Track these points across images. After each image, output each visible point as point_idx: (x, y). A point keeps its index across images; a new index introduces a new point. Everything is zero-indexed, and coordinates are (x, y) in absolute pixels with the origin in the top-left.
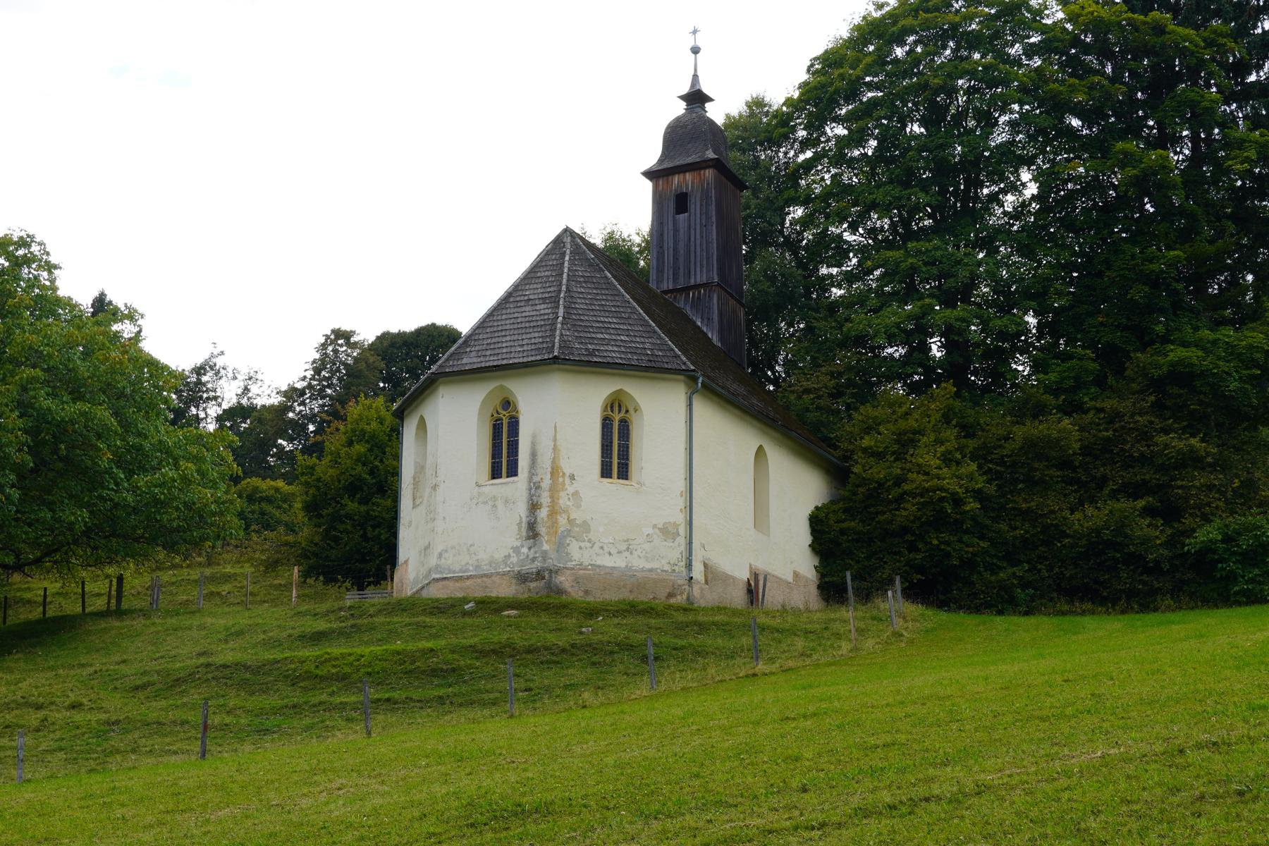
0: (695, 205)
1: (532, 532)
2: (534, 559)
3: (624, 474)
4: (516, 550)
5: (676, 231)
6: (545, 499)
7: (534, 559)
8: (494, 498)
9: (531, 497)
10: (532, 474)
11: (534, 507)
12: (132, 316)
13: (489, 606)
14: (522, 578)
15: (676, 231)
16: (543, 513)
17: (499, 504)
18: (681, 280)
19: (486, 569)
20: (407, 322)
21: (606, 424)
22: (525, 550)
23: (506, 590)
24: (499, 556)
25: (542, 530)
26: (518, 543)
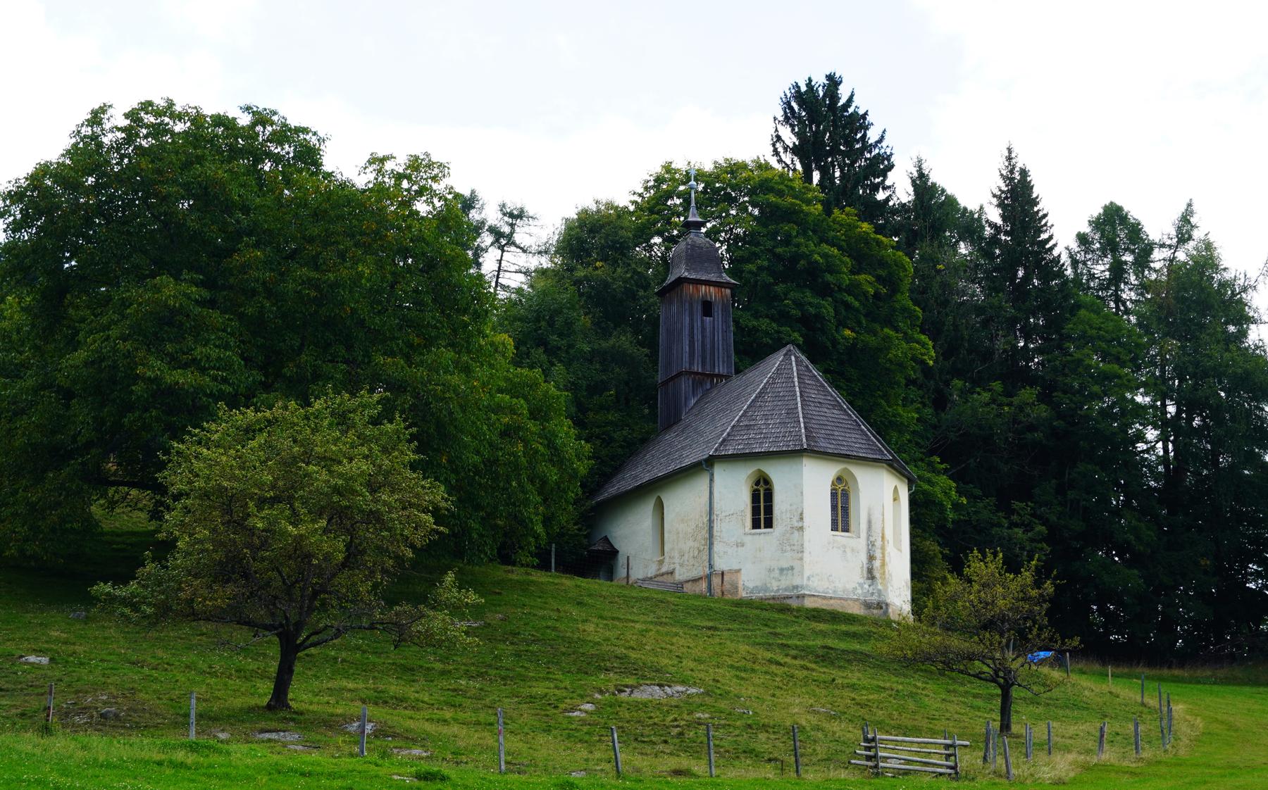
0: (718, 312)
1: (871, 575)
2: (872, 594)
3: (769, 524)
4: (861, 585)
5: (703, 329)
6: (878, 554)
7: (872, 594)
8: (844, 546)
9: (869, 550)
10: (869, 536)
11: (871, 558)
12: (96, 118)
13: (834, 617)
14: (868, 605)
15: (703, 329)
16: (877, 564)
17: (848, 550)
18: (708, 367)
19: (840, 594)
20: (30, 169)
21: (834, 495)
22: (866, 586)
23: (857, 610)
24: (850, 586)
25: (877, 575)
26: (862, 581)
